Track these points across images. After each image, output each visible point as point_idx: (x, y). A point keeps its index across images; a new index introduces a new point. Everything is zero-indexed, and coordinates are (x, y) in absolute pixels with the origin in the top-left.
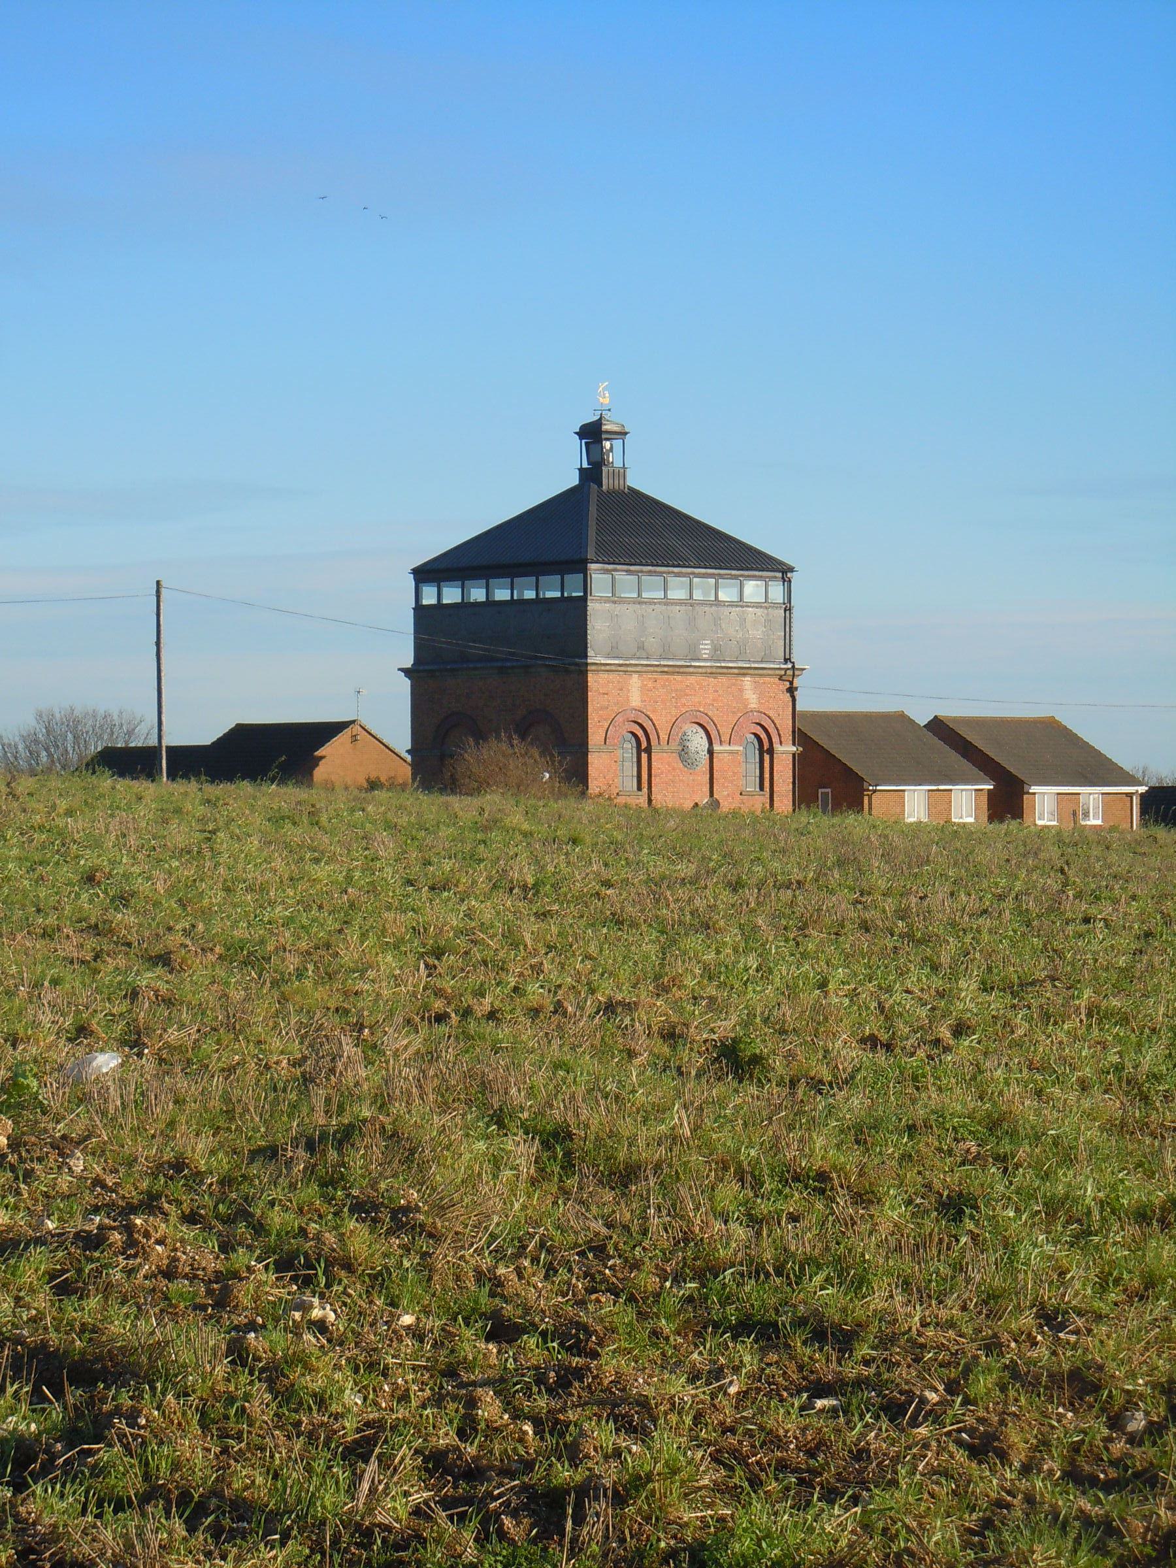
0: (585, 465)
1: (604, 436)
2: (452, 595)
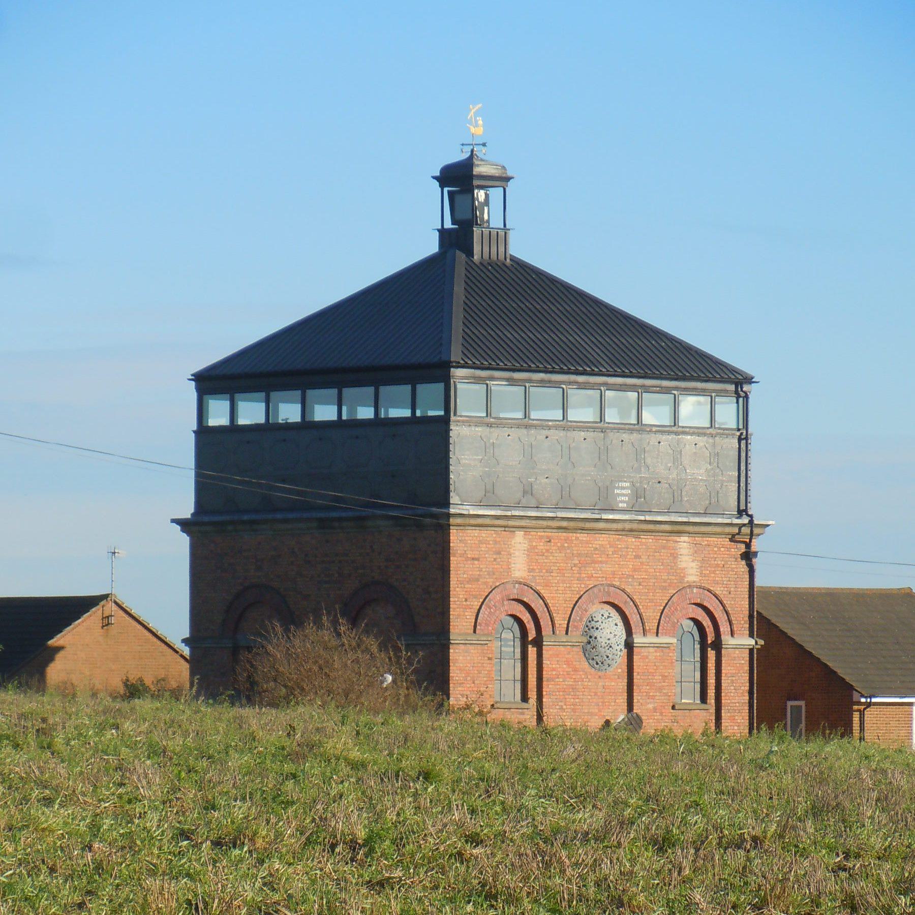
0: (448, 225)
2: (251, 412)
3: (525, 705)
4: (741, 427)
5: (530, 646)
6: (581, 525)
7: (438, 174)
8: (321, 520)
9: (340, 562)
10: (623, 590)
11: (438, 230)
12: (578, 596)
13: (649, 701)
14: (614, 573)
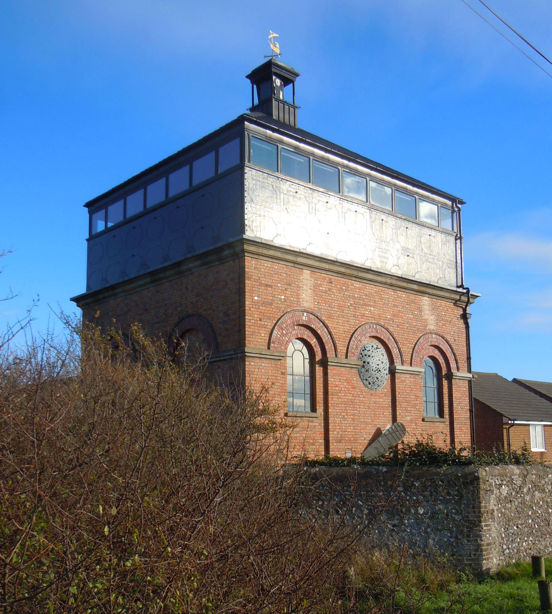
3: (314, 415)
4: (455, 230)
5: (317, 365)
6: (355, 273)
10: (387, 329)
13: (407, 414)
14: (379, 315)
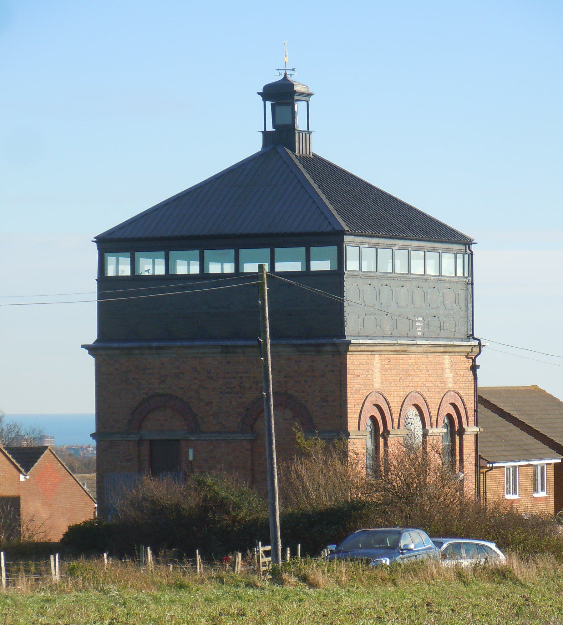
0: (270, 128)
1: (296, 97)
2: (152, 266)
4: (466, 275)
7: (262, 91)
8: (223, 347)
9: (241, 377)
11: (262, 132)
12: (402, 401)
